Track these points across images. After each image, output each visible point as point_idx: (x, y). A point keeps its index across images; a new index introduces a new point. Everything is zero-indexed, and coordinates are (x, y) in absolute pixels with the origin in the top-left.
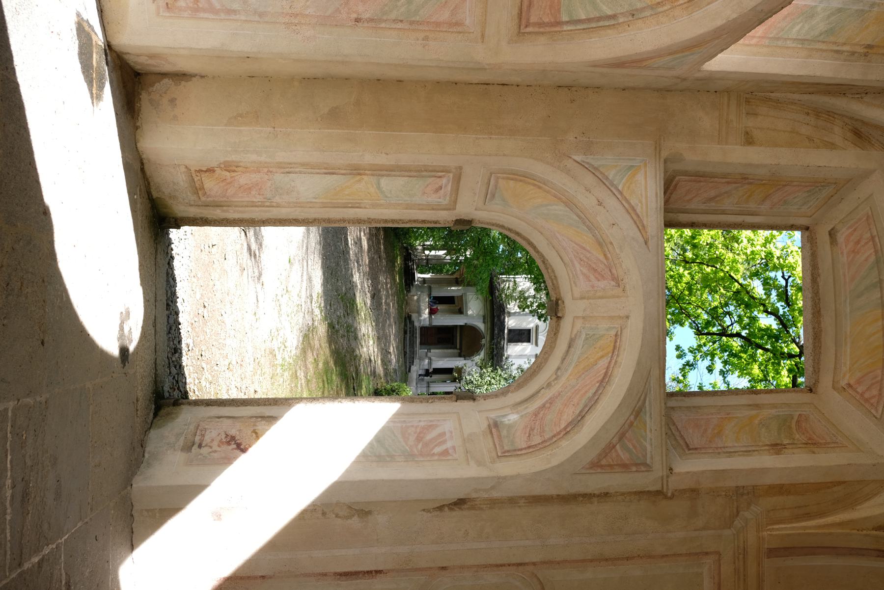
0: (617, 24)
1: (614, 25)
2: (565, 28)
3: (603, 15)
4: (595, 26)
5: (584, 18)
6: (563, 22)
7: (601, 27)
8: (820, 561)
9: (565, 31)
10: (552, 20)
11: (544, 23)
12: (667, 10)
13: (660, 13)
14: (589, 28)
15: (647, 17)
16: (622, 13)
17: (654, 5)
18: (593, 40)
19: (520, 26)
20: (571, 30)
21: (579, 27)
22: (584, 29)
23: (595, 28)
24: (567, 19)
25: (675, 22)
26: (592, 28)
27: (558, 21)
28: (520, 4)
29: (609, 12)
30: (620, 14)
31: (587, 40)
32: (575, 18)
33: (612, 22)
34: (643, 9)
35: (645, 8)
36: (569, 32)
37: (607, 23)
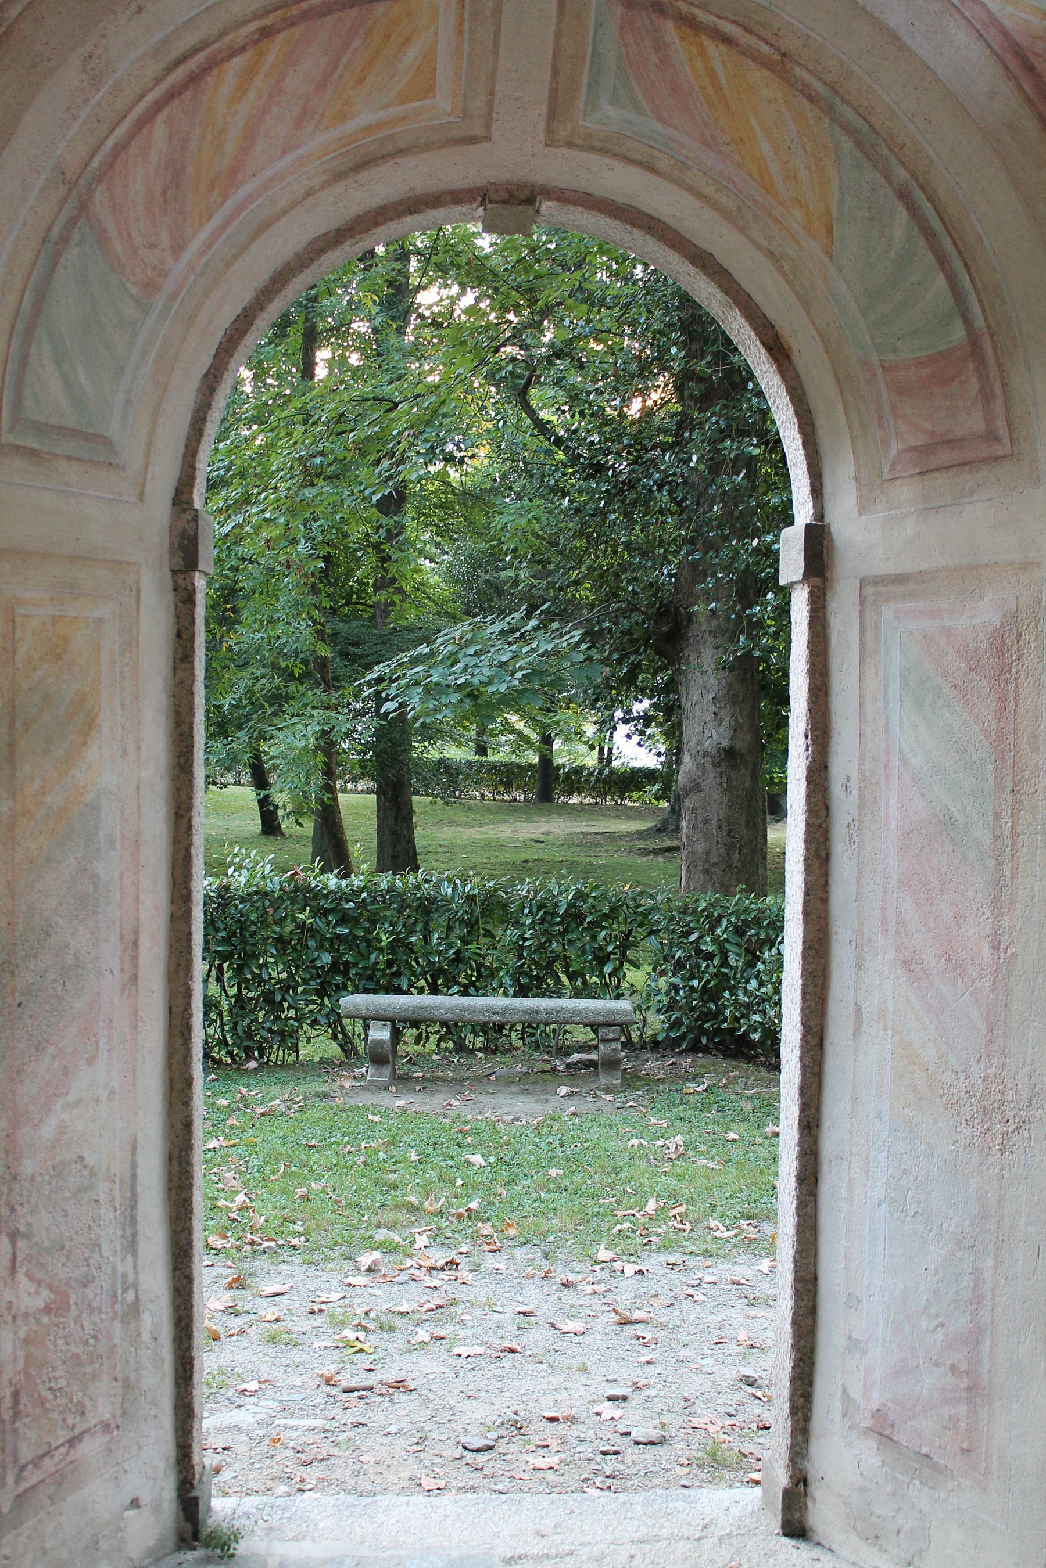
0: (916, 180)
1: (922, 188)
2: (980, 323)
3: (916, 230)
4: (948, 240)
5: (942, 276)
6: (969, 335)
7: (942, 219)
8: (7, 378)
9: (986, 320)
10: (971, 366)
11: (982, 389)
12: (809, 70)
13: (825, 84)
14: (960, 253)
15: (855, 109)
16: (886, 178)
17: (820, 108)
18: (980, 229)
19: (997, 458)
20: (980, 301)
21: (967, 283)
22: (966, 266)
23: (951, 236)
24: (959, 324)
25: (813, 35)
26: (955, 244)
27: (969, 349)
28: (951, 473)
29: (901, 213)
30: (890, 183)
31: (987, 243)
32: (951, 303)
33: (918, 195)
34: (849, 130)
35: (843, 128)
36: (986, 306)
37: (928, 208)
